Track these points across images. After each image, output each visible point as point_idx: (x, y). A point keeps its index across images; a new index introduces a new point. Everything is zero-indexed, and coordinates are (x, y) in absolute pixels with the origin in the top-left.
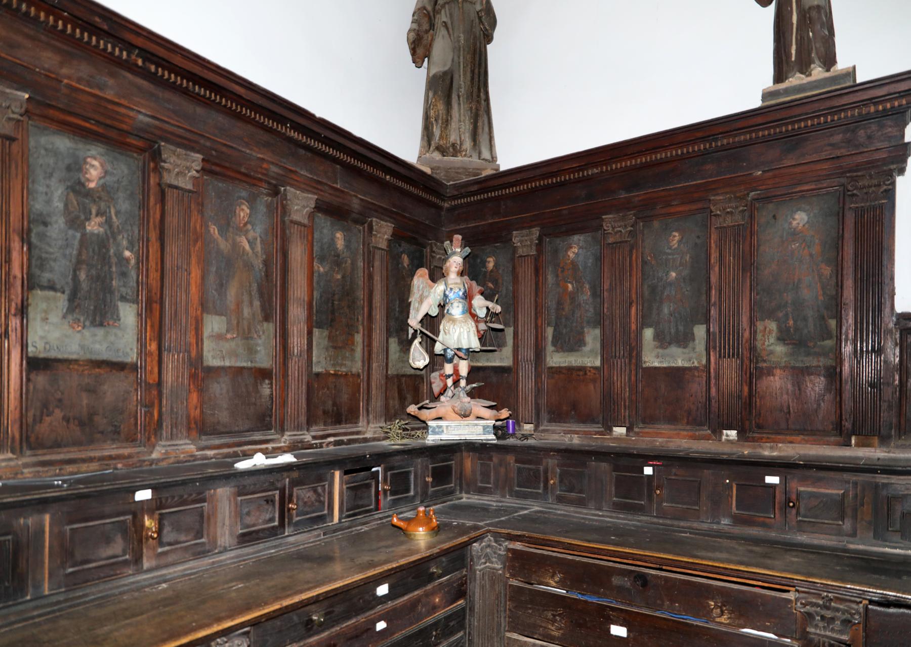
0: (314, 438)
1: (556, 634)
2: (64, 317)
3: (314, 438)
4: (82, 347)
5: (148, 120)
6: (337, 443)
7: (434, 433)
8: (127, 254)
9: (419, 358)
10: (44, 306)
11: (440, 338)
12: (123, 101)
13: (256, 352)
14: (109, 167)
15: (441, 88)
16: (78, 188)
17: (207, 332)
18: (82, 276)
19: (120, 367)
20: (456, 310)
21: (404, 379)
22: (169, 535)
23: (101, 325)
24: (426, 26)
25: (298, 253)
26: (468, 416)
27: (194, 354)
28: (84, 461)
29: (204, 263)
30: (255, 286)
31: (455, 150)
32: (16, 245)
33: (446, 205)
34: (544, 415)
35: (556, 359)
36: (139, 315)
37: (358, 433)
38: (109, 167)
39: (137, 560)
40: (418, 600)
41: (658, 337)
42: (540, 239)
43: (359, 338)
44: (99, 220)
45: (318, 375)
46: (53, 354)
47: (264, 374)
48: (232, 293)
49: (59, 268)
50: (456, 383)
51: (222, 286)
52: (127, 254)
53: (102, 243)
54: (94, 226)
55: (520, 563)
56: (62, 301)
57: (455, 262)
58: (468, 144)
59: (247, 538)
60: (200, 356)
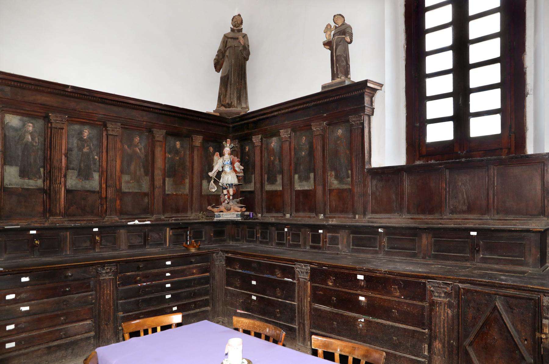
0: (166, 218)
1: (238, 285)
2: (77, 177)
3: (166, 218)
4: (82, 186)
5: (102, 116)
6: (175, 220)
7: (217, 217)
8: (96, 157)
9: (214, 189)
10: (71, 174)
11: (221, 181)
12: (95, 112)
13: (142, 187)
14: (90, 132)
15: (225, 82)
16: (81, 139)
17: (123, 180)
18: (82, 165)
19: (94, 192)
20: (227, 169)
21: (210, 197)
22: (104, 242)
23: (88, 179)
24: (221, 57)
25: (159, 152)
26: (230, 210)
27: (118, 188)
28: (82, 220)
29: (101, 166)
30: (141, 164)
31: (229, 105)
32: (63, 157)
33: (231, 126)
34: (264, 210)
35: (268, 187)
36: (100, 176)
37: (187, 217)
38: (90, 132)
39: (94, 249)
40: (185, 269)
41: (300, 178)
42: (261, 139)
43: (187, 181)
44: (87, 148)
45: (168, 195)
46: (73, 189)
47: (146, 194)
48: (132, 167)
49: (75, 164)
50: (229, 198)
51: (129, 165)
52: (96, 157)
53: (88, 154)
54: (85, 150)
55: (229, 261)
56: (76, 172)
57: (227, 150)
58: (235, 102)
59: (131, 247)
60: (121, 188)
